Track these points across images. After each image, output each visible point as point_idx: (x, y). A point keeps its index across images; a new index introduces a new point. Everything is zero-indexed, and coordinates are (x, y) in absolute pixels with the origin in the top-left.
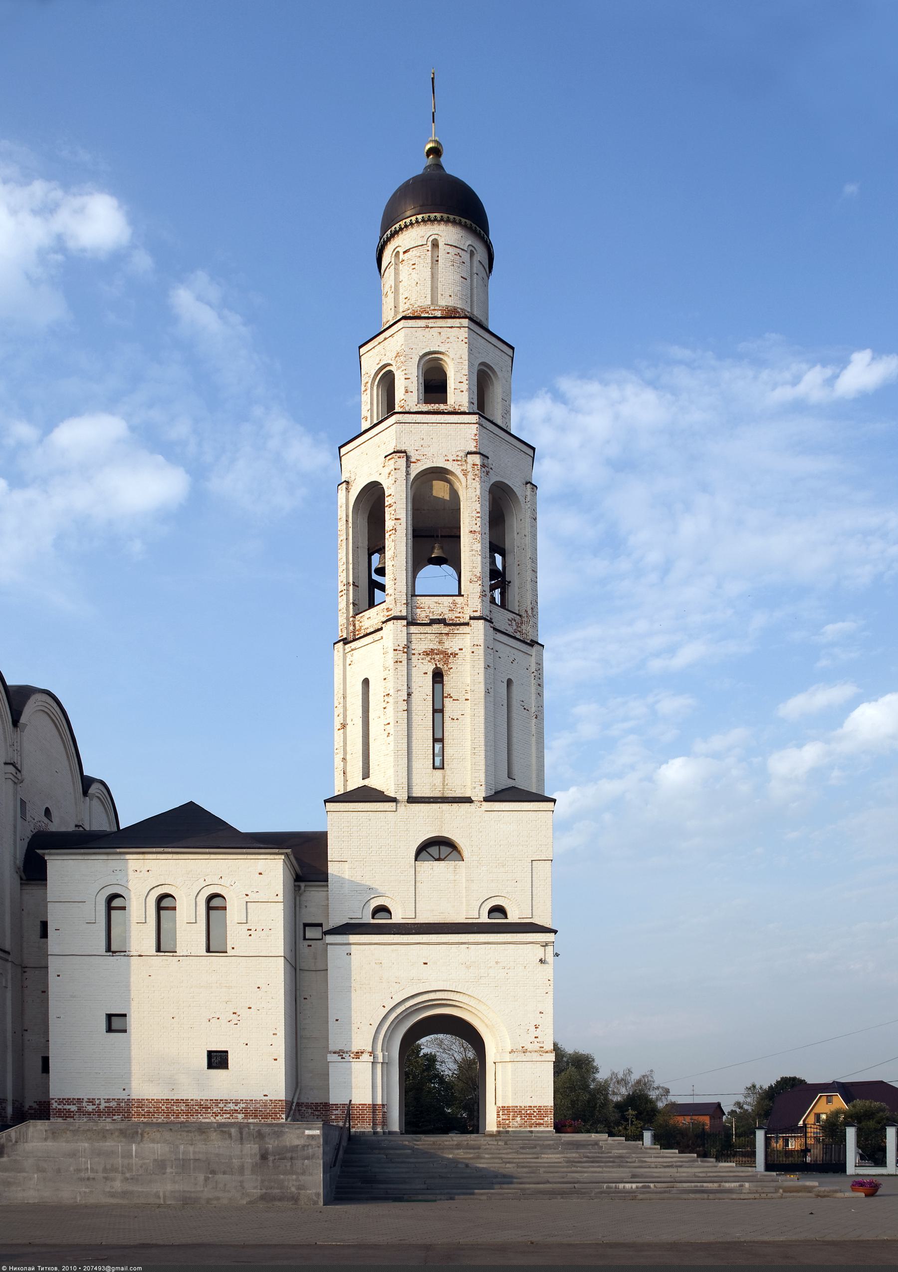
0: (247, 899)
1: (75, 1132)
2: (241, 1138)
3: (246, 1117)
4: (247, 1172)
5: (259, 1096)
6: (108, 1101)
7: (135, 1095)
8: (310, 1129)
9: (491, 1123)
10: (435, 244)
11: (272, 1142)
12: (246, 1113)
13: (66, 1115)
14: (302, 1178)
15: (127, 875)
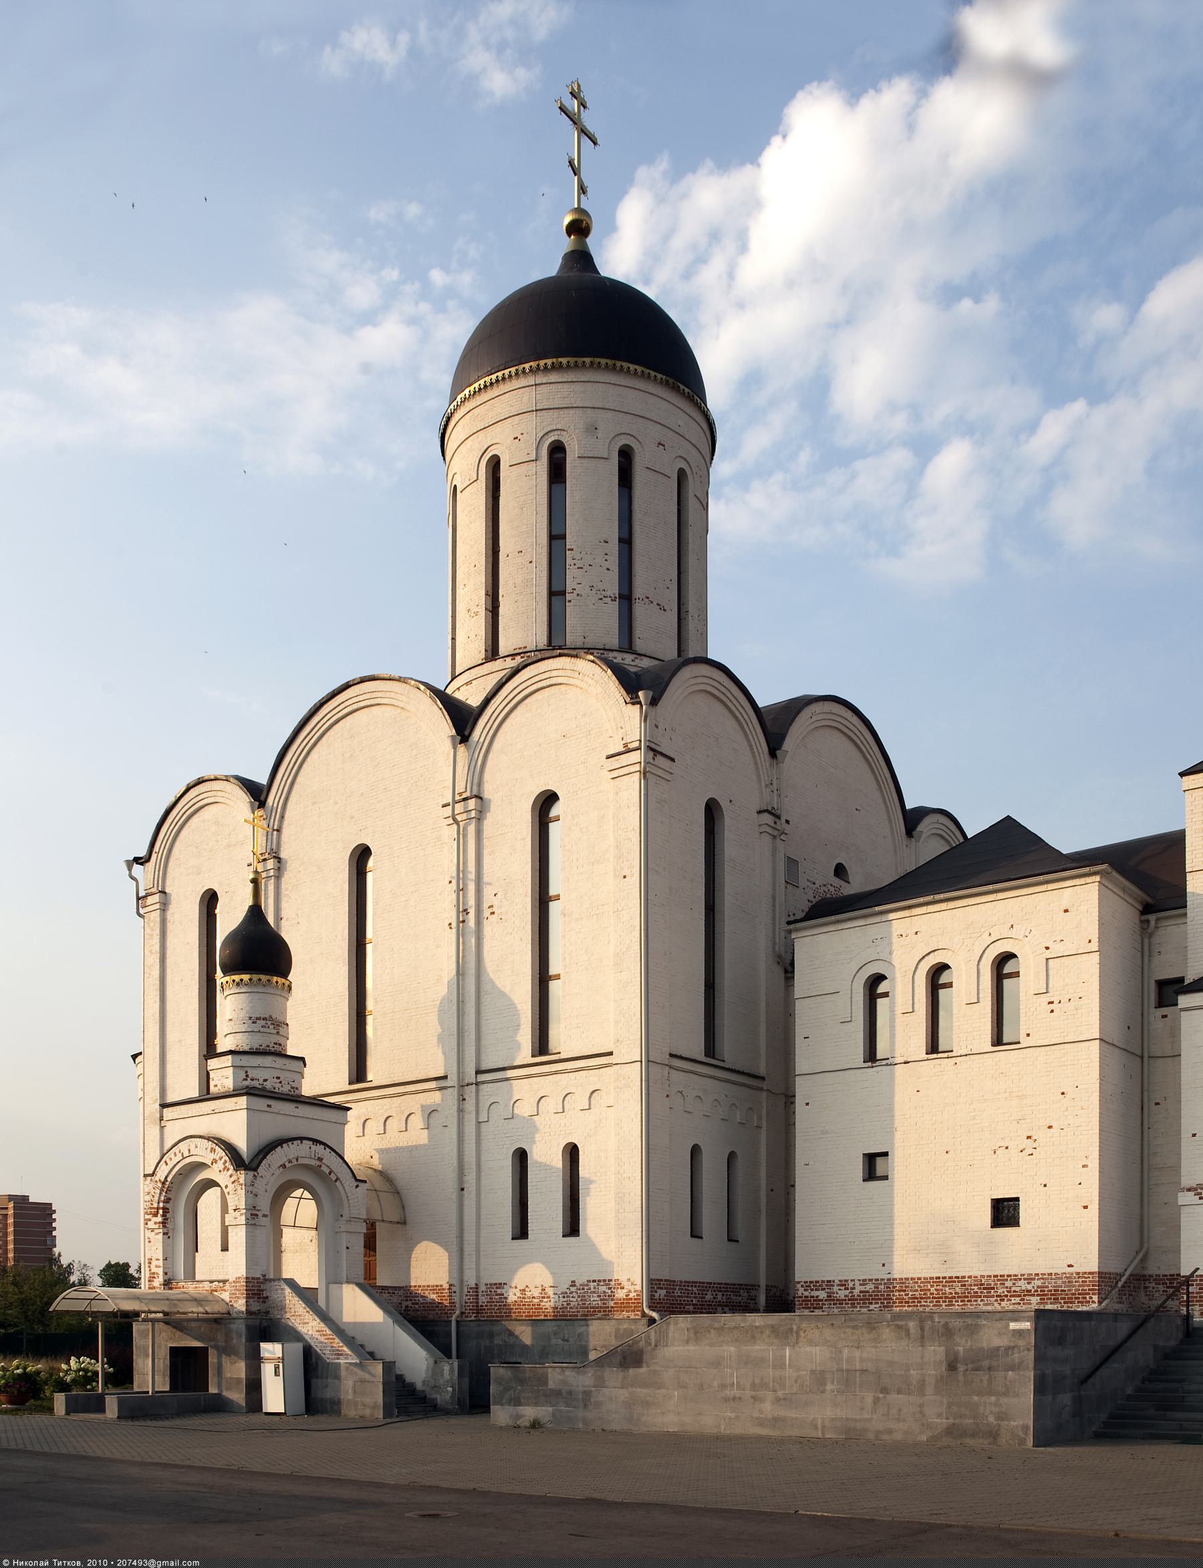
0: (1048, 954)
1: (720, 1330)
2: (922, 1337)
3: (1042, 1301)
4: (929, 1390)
5: (1060, 1268)
6: (864, 1282)
7: (896, 1275)
8: (1016, 1320)
11: (963, 1341)
12: (1042, 1293)
13: (813, 1304)
14: (1004, 1400)
15: (890, 944)
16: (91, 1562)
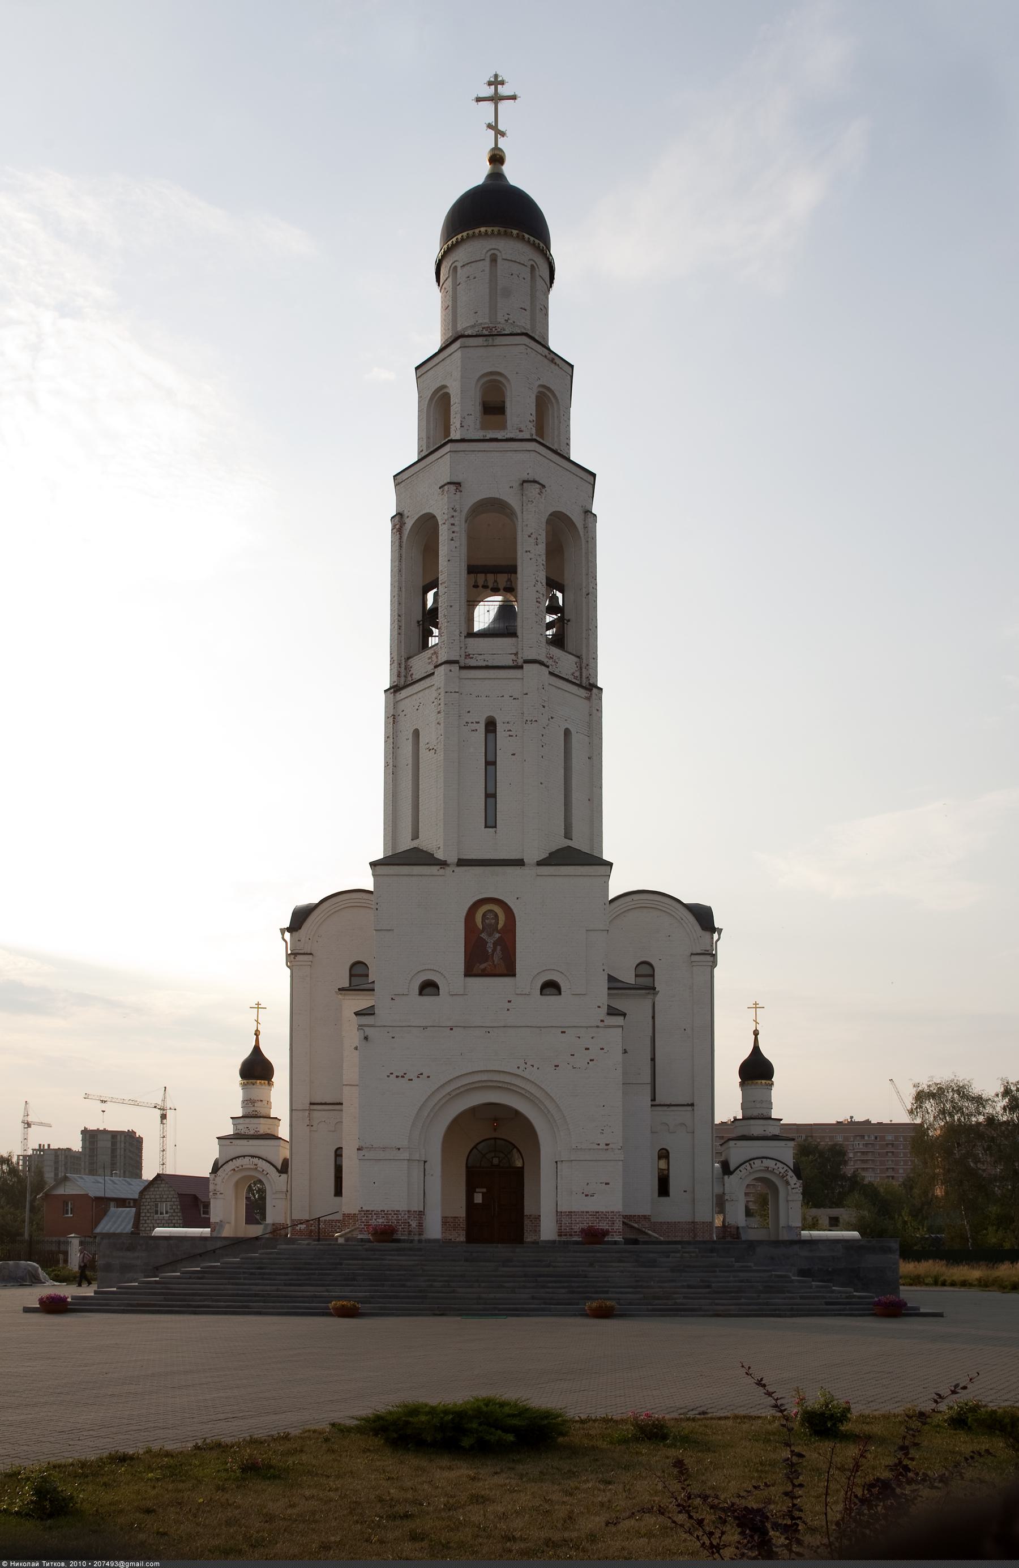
9: (548, 1231)
10: (494, 259)
16: (73, 1563)
